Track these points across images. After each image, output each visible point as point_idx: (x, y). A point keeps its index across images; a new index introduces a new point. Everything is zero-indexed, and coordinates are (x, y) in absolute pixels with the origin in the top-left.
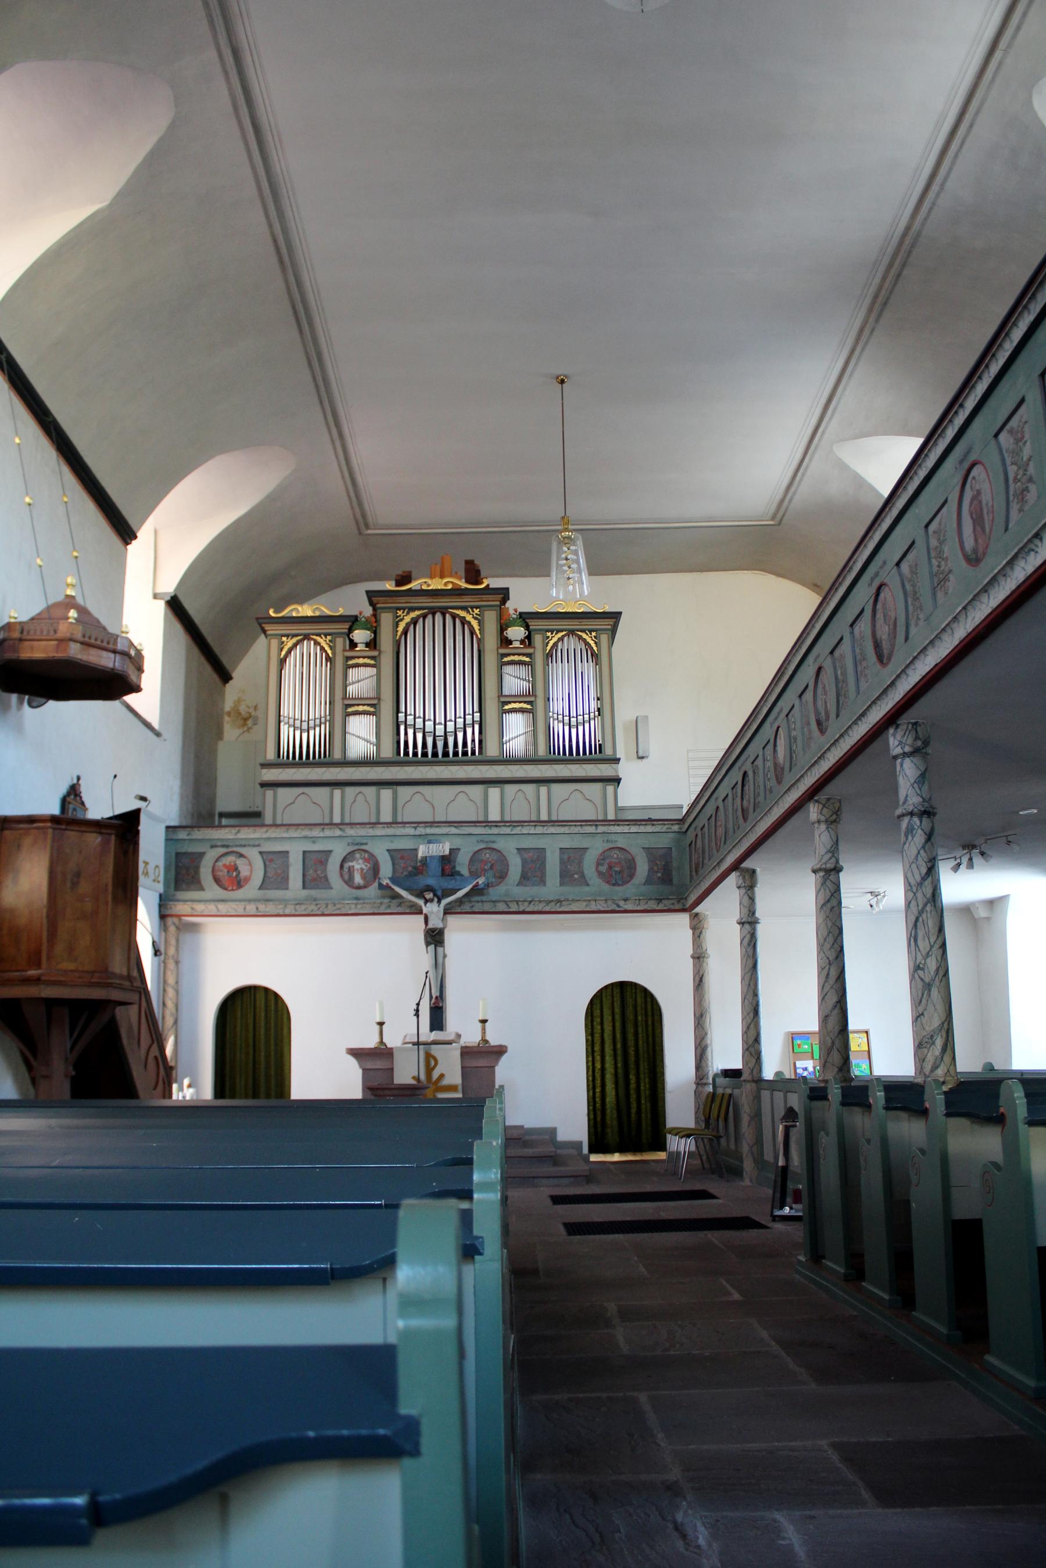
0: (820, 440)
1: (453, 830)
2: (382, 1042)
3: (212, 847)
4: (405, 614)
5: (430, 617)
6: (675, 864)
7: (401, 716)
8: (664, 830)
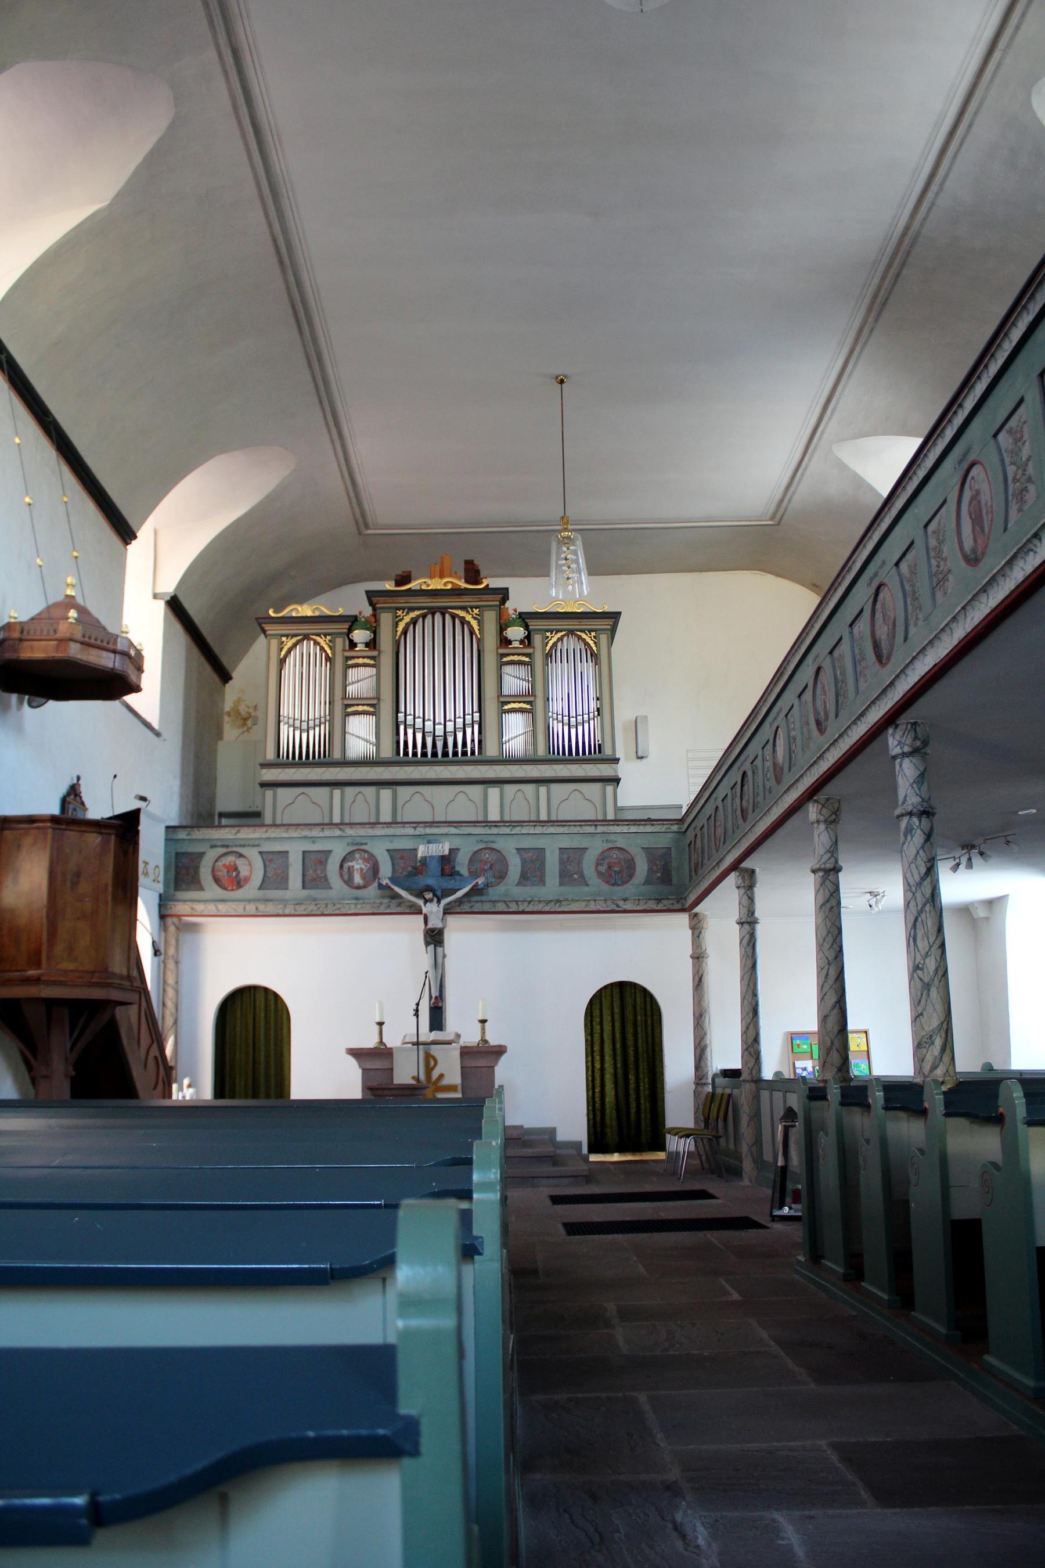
0: (819, 440)
1: (453, 830)
2: (381, 1042)
3: (212, 847)
4: (404, 614)
5: (430, 617)
6: (674, 864)
7: (401, 716)
8: (663, 830)
